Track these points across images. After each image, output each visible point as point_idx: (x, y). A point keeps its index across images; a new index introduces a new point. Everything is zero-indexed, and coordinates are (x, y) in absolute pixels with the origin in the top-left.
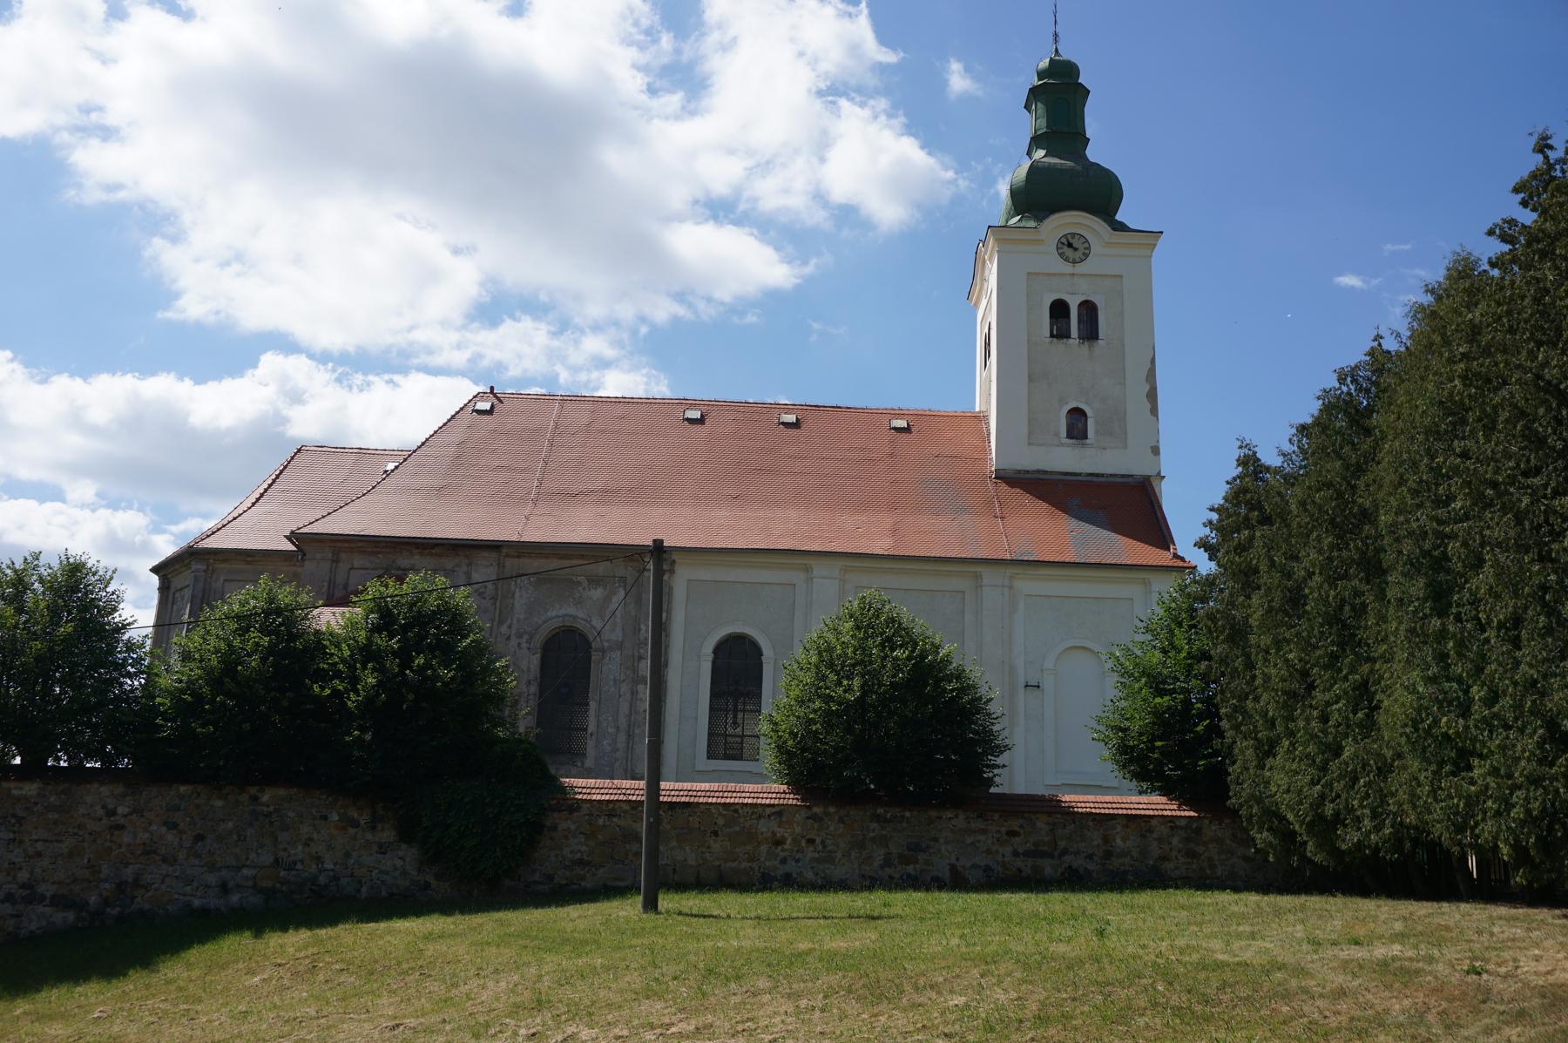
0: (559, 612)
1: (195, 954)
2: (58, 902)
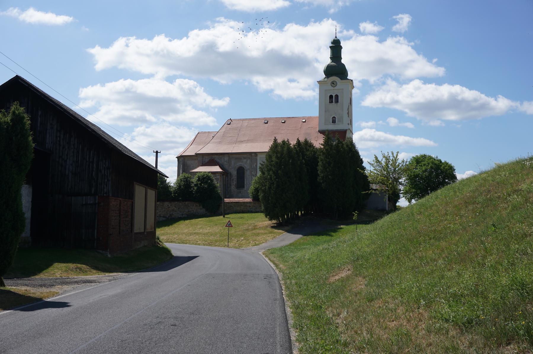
0: (239, 164)
1: (177, 223)
2: (164, 217)
